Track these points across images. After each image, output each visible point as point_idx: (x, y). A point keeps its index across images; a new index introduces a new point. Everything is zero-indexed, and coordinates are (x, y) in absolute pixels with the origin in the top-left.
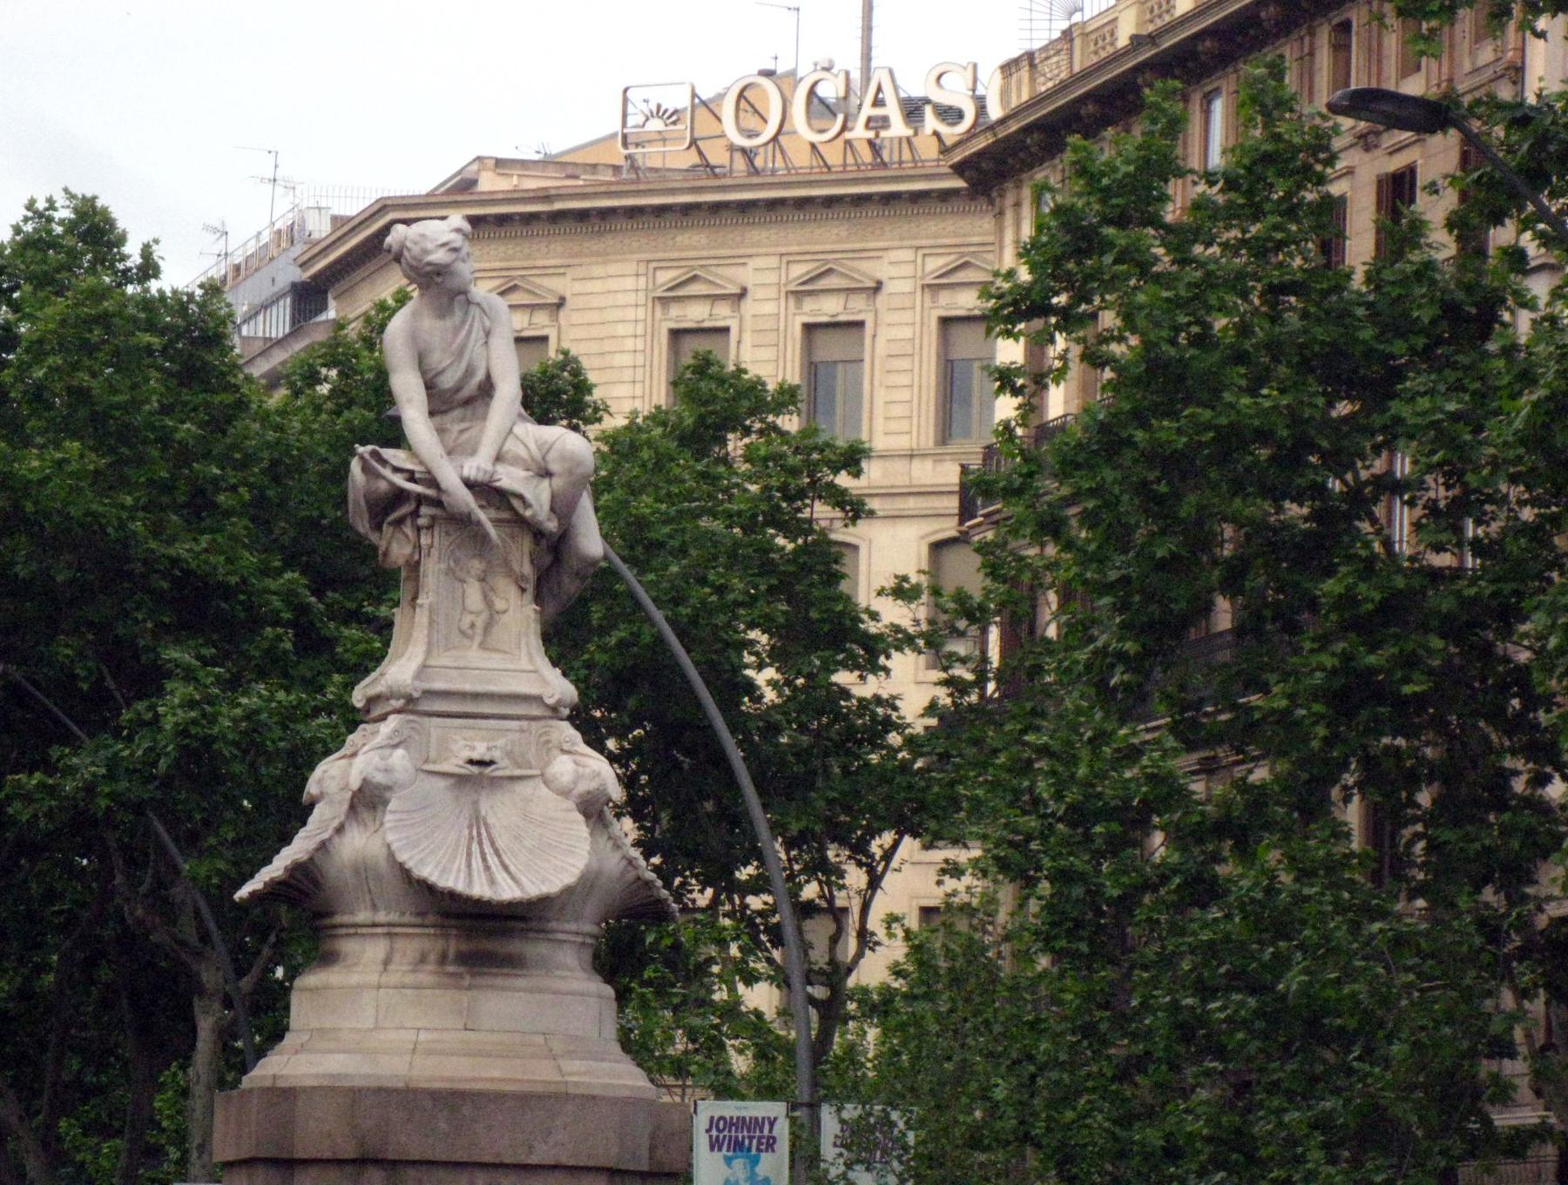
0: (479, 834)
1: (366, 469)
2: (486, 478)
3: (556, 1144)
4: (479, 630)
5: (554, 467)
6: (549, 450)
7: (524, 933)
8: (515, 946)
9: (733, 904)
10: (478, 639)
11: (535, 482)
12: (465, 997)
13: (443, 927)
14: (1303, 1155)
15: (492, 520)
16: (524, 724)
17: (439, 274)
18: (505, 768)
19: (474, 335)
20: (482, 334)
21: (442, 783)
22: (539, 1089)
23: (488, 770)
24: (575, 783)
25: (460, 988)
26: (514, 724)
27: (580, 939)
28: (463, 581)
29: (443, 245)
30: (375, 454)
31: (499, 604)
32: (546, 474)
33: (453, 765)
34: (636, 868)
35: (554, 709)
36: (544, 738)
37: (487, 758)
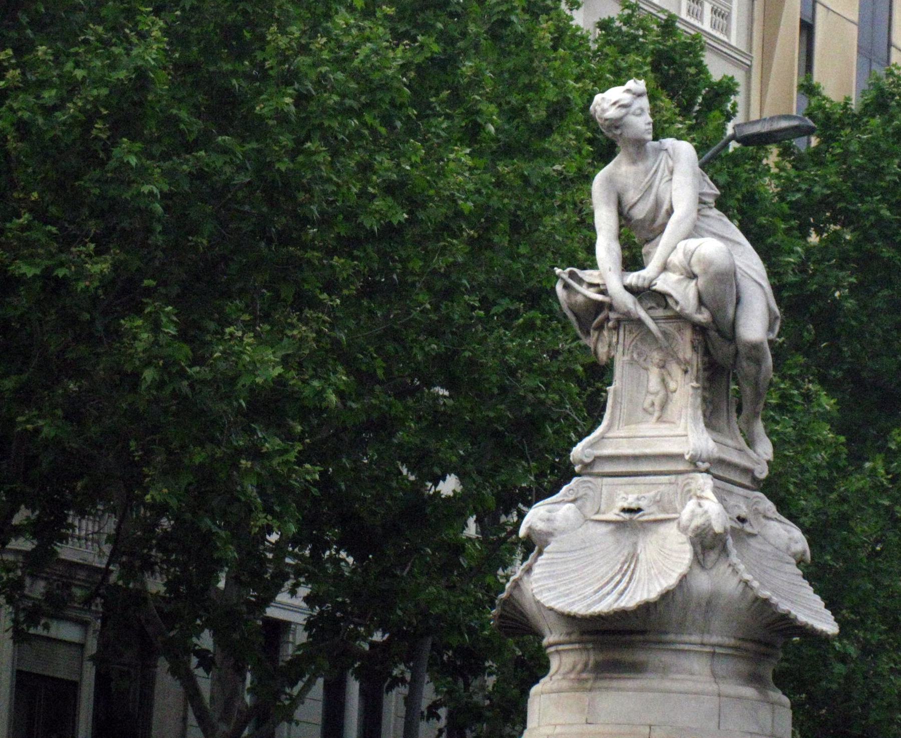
0: (626, 571)
1: (566, 286)
2: (646, 284)
4: (657, 408)
5: (696, 270)
6: (692, 256)
7: (646, 645)
8: (640, 656)
9: (252, 596)
10: (657, 414)
11: (685, 284)
12: (586, 697)
15: (654, 319)
16: (673, 478)
17: (617, 128)
18: (651, 513)
19: (659, 174)
20: (667, 173)
21: (604, 529)
23: (636, 516)
25: (585, 690)
27: (707, 649)
28: (647, 369)
29: (615, 104)
30: (572, 275)
31: (672, 385)
32: (693, 276)
33: (613, 515)
34: (752, 588)
36: (687, 488)
37: (634, 506)
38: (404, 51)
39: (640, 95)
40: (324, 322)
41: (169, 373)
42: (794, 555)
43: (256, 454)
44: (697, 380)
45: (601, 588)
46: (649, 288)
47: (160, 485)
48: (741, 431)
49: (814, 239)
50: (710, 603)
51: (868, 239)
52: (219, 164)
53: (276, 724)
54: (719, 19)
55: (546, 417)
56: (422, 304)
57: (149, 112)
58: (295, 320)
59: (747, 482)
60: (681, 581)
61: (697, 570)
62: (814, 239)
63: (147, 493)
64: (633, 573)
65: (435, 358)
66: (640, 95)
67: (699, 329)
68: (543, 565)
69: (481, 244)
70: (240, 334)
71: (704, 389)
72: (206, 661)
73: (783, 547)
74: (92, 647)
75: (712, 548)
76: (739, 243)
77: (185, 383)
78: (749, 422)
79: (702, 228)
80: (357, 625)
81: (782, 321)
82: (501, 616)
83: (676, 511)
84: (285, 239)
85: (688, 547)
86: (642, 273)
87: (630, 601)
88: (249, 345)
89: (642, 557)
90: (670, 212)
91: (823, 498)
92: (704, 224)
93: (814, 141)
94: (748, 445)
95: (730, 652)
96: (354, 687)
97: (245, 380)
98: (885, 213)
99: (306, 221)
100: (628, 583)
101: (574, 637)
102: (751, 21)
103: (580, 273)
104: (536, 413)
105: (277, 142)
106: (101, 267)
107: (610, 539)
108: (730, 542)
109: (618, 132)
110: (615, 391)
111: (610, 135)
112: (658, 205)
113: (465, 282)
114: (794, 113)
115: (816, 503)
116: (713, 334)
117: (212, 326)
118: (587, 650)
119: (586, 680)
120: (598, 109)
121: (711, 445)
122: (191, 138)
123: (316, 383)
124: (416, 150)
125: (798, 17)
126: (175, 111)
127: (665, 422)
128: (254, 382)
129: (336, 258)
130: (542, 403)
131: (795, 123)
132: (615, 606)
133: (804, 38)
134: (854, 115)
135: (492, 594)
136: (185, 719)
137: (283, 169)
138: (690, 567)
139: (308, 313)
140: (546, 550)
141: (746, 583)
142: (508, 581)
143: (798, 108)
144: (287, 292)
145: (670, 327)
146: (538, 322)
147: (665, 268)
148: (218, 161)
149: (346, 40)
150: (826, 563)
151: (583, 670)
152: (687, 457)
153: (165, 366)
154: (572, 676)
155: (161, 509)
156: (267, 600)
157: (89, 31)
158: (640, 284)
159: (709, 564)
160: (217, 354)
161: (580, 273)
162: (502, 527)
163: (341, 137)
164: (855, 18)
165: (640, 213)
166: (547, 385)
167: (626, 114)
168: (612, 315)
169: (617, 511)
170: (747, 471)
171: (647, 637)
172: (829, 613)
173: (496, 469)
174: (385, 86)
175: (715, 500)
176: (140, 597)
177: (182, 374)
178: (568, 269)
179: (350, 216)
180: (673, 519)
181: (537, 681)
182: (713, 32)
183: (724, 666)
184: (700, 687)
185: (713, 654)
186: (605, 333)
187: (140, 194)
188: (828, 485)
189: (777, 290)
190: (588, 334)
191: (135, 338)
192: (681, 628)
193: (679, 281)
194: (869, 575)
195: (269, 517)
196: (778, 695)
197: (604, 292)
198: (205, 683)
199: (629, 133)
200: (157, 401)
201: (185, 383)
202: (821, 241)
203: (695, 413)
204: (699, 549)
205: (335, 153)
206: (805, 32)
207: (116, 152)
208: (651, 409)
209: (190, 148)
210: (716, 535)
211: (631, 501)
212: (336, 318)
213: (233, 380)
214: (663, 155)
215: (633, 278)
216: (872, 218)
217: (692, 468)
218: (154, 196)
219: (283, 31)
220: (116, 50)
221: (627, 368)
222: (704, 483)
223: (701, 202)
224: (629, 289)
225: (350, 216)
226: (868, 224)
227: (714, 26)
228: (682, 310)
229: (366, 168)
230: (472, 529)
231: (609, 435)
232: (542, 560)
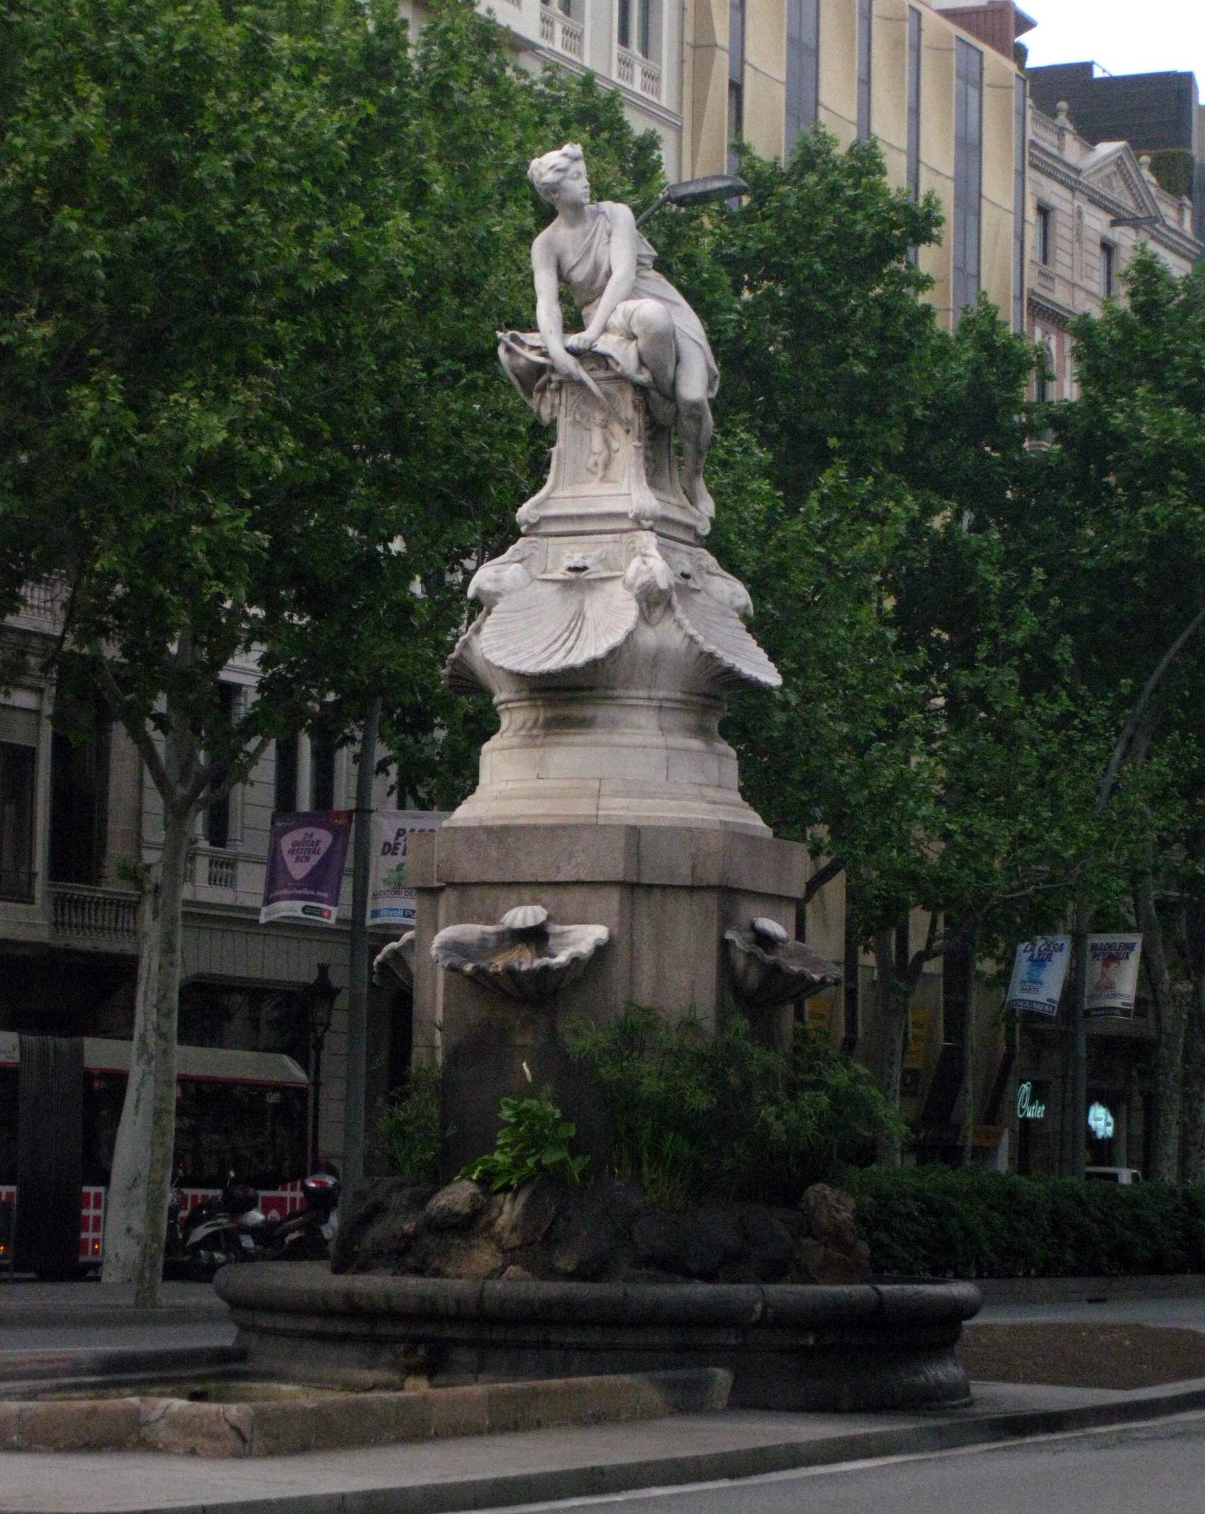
1: (509, 350)
2: (587, 346)
3: (577, 864)
4: (600, 467)
5: (636, 331)
7: (595, 701)
8: (588, 712)
10: (600, 474)
12: (537, 753)
13: (530, 699)
14: (197, 732)
15: (596, 380)
16: (617, 536)
17: (555, 192)
18: (597, 571)
20: (605, 235)
21: (551, 588)
22: (572, 821)
24: (635, 578)
25: (535, 746)
26: (609, 537)
27: (655, 703)
28: (589, 430)
29: (552, 168)
30: (514, 338)
31: (615, 445)
33: (559, 574)
34: (696, 643)
35: (637, 519)
37: (580, 565)
38: (341, 117)
39: (576, 159)
40: (269, 388)
41: (116, 441)
42: (737, 610)
43: (207, 521)
44: (639, 438)
45: (550, 645)
46: (590, 349)
47: (110, 553)
48: (685, 492)
49: (747, 295)
50: (656, 659)
51: (800, 292)
52: (161, 228)
53: (232, 785)
54: (649, 81)
55: (491, 477)
56: (368, 365)
57: (90, 179)
58: (240, 386)
59: (690, 538)
60: (627, 637)
61: (643, 627)
62: (747, 295)
63: (96, 562)
64: (580, 631)
65: (382, 422)
66: (576, 159)
67: (639, 388)
68: (494, 624)
69: (422, 307)
70: (184, 401)
71: (646, 448)
72: (161, 721)
73: (727, 602)
74: (48, 709)
75: (657, 604)
76: (676, 304)
77: (133, 450)
78: (691, 480)
79: (641, 290)
80: (308, 687)
81: (721, 380)
82: (451, 676)
83: (621, 569)
84: (228, 307)
85: (634, 604)
86: (583, 335)
87: (578, 658)
88: (194, 410)
89: (589, 614)
90: (609, 274)
91: (762, 550)
92: (644, 285)
93: (746, 200)
94: (692, 503)
95: (678, 705)
96: (306, 744)
97: (192, 447)
98: (819, 267)
99: (247, 286)
100: (576, 640)
101: (524, 694)
102: (681, 82)
103: (522, 336)
104: (480, 474)
105: (217, 206)
106: (45, 330)
107: (558, 598)
108: (675, 598)
109: (556, 196)
110: (559, 453)
111: (548, 199)
112: (596, 267)
113: (410, 343)
114: (725, 172)
115: (756, 553)
116: (653, 393)
117: (159, 394)
118: (537, 707)
119: (537, 736)
120: (536, 173)
121: (655, 503)
122: (133, 208)
123: (263, 450)
124: (354, 215)
125: (727, 78)
126: (115, 178)
127: (608, 481)
128: (200, 448)
129: (278, 322)
130: (487, 462)
131: (728, 183)
132: (564, 664)
133: (734, 100)
134: (783, 174)
135: (443, 653)
136: (141, 782)
137: (223, 232)
138: (637, 624)
139: (253, 379)
140: (494, 609)
141: (691, 638)
142: (457, 641)
143: (730, 167)
144: (230, 357)
145: (612, 388)
146: (481, 382)
147: (605, 329)
148: (160, 226)
149: (285, 108)
150: (767, 612)
151: (532, 728)
152: (631, 516)
153: (112, 434)
154: (523, 732)
155: (114, 577)
156: (219, 665)
157: (26, 99)
158: (581, 345)
159: (653, 620)
160: (163, 421)
161: (522, 336)
162: (449, 589)
163: (281, 204)
164: (783, 77)
165: (579, 275)
166: (491, 445)
167: (563, 179)
168: (554, 377)
169: (563, 570)
170: (689, 528)
171: (594, 693)
172: (772, 665)
173: (442, 529)
174: (323, 149)
175: (660, 557)
176: (95, 662)
177: (129, 441)
178: (510, 332)
179: (290, 280)
180: (618, 577)
181: (487, 739)
182: (644, 94)
183: (669, 719)
184: (649, 741)
185: (660, 708)
186: (548, 395)
187: (82, 260)
188: (766, 537)
189: (714, 344)
190: (530, 395)
191: (82, 407)
192: (628, 682)
193: (619, 343)
194: (808, 624)
195: (222, 586)
196: (724, 747)
197: (545, 355)
198: (160, 743)
199: (567, 197)
200: (105, 469)
201: (133, 450)
202: (754, 298)
203: (638, 474)
204: (644, 605)
205: (276, 219)
206: (734, 94)
207: (57, 218)
208: (594, 469)
209: (131, 217)
210: (660, 592)
211: (576, 560)
212: (282, 384)
213: (179, 447)
214: (601, 219)
215: (574, 340)
216: (806, 272)
217: (635, 526)
218: (97, 262)
219: (221, 94)
220: (56, 119)
221: (569, 428)
222: (648, 540)
223: (639, 264)
224: (569, 350)
225: (290, 280)
226: (802, 277)
227: (644, 88)
228: (623, 371)
229: (304, 234)
230: (417, 587)
231: (556, 494)
232: (490, 620)
